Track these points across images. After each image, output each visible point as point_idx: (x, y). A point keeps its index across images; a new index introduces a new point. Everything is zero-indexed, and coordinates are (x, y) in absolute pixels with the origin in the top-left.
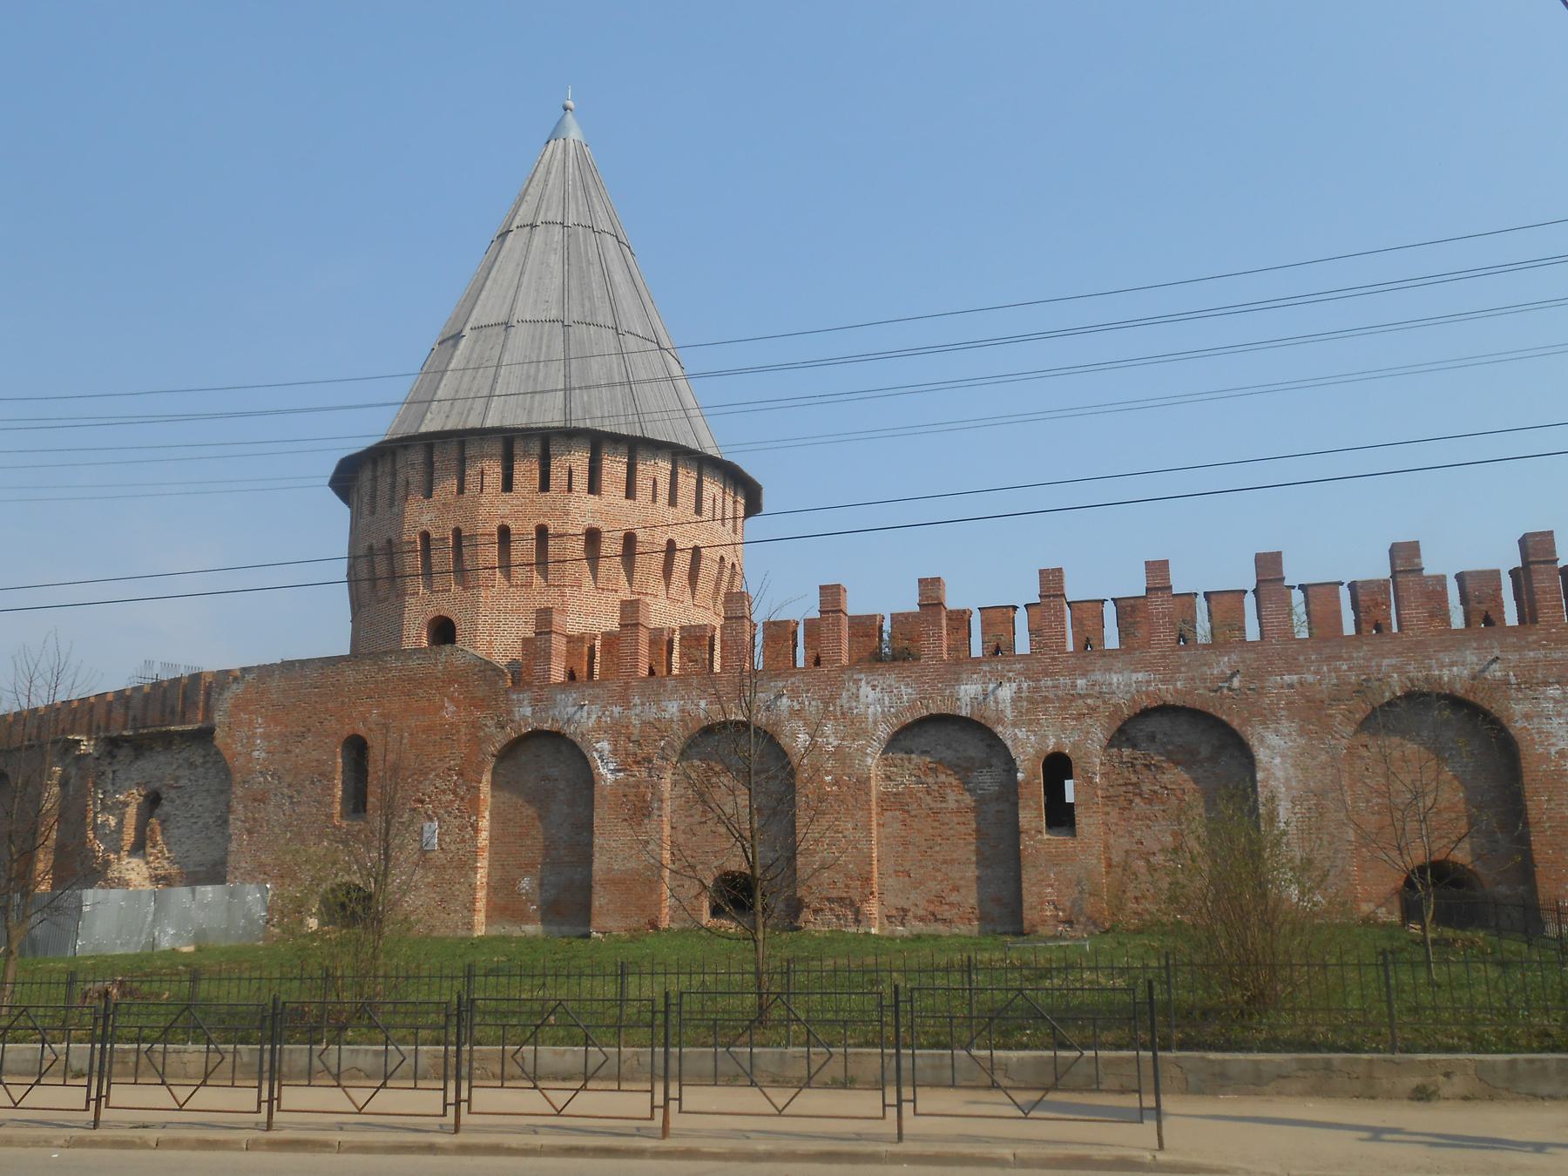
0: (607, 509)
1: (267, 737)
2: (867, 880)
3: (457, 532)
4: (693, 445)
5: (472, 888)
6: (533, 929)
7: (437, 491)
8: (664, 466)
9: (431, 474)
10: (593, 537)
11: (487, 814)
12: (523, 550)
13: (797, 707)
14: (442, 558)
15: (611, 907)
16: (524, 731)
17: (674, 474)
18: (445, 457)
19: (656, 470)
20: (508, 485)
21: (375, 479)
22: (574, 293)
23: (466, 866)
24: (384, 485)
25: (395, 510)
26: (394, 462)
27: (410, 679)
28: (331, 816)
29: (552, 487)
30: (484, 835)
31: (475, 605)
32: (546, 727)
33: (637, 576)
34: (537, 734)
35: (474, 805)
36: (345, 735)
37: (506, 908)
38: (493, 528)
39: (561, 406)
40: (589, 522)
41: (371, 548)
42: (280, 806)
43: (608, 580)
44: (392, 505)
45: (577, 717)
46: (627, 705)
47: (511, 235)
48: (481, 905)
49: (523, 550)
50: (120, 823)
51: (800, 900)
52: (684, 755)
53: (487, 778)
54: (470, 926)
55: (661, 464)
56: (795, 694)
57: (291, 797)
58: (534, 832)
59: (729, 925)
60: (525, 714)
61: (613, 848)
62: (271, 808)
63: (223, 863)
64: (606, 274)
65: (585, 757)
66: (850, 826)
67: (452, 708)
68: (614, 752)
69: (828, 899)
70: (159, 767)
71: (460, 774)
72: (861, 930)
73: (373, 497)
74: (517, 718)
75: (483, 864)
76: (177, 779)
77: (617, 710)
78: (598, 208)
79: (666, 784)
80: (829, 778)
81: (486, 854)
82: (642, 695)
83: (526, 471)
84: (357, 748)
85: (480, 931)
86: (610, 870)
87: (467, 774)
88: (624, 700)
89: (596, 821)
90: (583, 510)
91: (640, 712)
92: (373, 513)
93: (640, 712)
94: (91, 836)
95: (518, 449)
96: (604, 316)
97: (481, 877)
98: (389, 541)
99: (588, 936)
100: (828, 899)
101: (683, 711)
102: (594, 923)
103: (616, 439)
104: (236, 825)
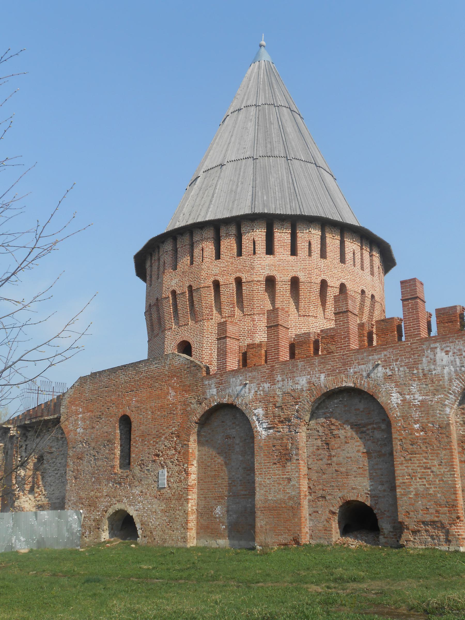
0: (281, 264)
1: (84, 419)
2: (453, 506)
4: (337, 218)
5: (186, 513)
6: (223, 542)
7: (180, 265)
9: (176, 258)
10: (270, 282)
11: (195, 463)
12: (228, 291)
13: (390, 373)
15: (268, 527)
16: (212, 405)
19: (310, 236)
20: (218, 256)
23: (182, 498)
25: (159, 280)
27: (152, 377)
28: (113, 467)
29: (244, 253)
31: (202, 332)
32: (225, 401)
33: (302, 305)
34: (221, 407)
35: (185, 456)
36: (120, 416)
37: (208, 527)
38: (210, 283)
39: (250, 204)
40: (268, 272)
42: (89, 462)
45: (243, 392)
46: (273, 382)
47: (228, 118)
49: (228, 291)
51: (401, 523)
52: (313, 415)
53: (193, 438)
54: (185, 539)
55: (313, 231)
56: (387, 363)
57: (94, 456)
58: (222, 474)
59: (353, 543)
60: (214, 394)
61: (268, 485)
63: (64, 498)
64: (282, 128)
65: (248, 420)
66: (436, 463)
67: (173, 394)
68: (266, 415)
69: (423, 523)
71: (178, 436)
72: (452, 549)
74: (208, 397)
75: (193, 497)
77: (267, 385)
78: (278, 93)
79: (302, 435)
80: (417, 426)
81: (195, 490)
83: (229, 244)
84: (126, 422)
85: (192, 543)
86: (266, 500)
87: (181, 436)
88: (271, 379)
89: (257, 465)
90: (263, 265)
91: (282, 386)
93: (282, 386)
94: (14, 482)
97: (192, 504)
98: (157, 299)
99: (254, 548)
100: (423, 523)
101: (309, 383)
102: (257, 539)
103: (283, 219)
104: (70, 475)
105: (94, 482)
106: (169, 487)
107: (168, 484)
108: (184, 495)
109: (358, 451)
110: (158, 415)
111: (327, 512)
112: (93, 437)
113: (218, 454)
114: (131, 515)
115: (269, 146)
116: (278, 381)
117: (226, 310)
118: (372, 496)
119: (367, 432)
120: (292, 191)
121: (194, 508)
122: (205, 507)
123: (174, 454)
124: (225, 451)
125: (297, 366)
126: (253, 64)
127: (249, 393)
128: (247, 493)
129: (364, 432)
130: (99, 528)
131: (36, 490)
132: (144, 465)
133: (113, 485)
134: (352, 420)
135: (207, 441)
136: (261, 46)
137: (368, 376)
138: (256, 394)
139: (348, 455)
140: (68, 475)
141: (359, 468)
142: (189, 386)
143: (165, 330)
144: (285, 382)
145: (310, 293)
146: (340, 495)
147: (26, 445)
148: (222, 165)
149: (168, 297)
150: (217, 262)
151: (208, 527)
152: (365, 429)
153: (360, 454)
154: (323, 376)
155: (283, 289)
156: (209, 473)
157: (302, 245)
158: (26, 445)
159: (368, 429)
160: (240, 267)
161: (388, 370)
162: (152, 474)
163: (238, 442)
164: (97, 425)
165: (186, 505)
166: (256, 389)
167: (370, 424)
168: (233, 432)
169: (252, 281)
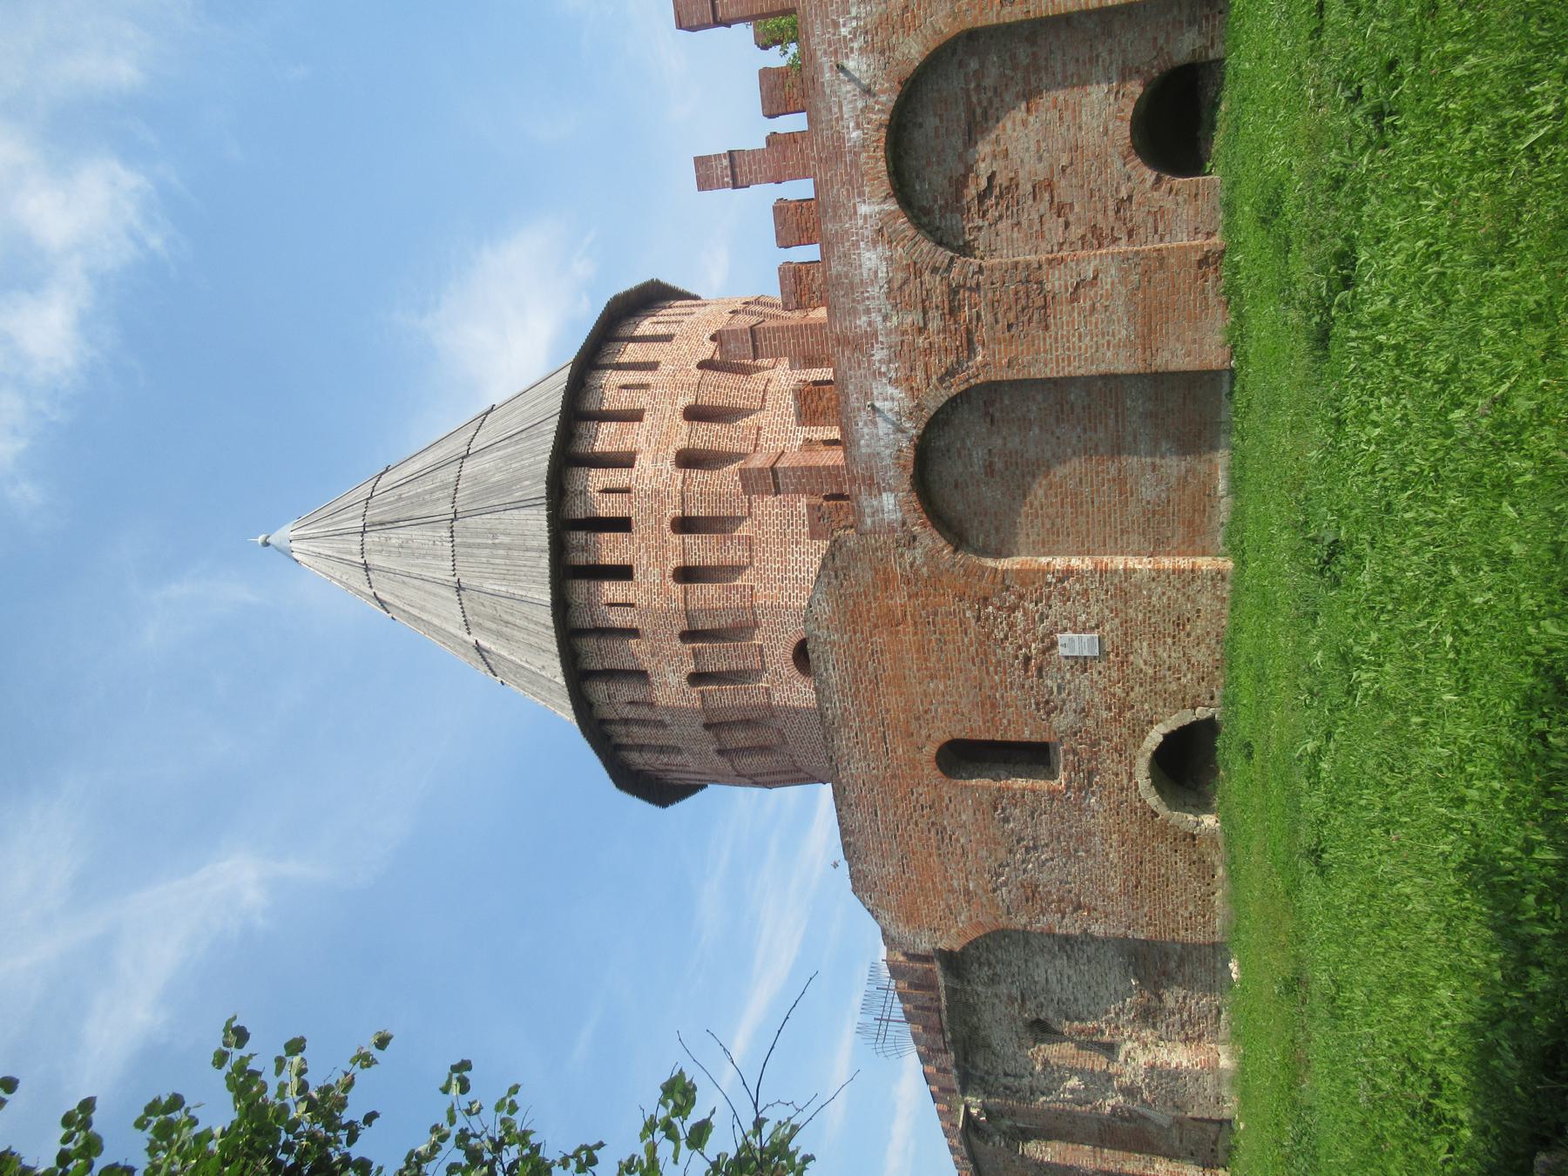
3: (687, 636)
8: (611, 379)
10: (688, 460)
11: (1044, 560)
12: (701, 549)
14: (717, 657)
15: (1189, 335)
17: (620, 367)
18: (597, 654)
19: (611, 388)
21: (641, 748)
22: (424, 512)
23: (1122, 588)
24: (640, 734)
25: (667, 719)
26: (612, 722)
28: (1053, 795)
30: (1075, 562)
31: (776, 610)
33: (741, 403)
35: (1023, 576)
38: (677, 589)
40: (669, 465)
41: (721, 752)
43: (744, 439)
44: (661, 724)
47: (380, 595)
48: (1184, 563)
49: (701, 549)
50: (1080, 1072)
57: (1027, 850)
60: (890, 505)
62: (1043, 878)
70: (998, 1023)
71: (985, 601)
73: (662, 749)
76: (1012, 999)
77: (879, 354)
82: (854, 312)
83: (610, 548)
84: (962, 756)
86: (1128, 343)
92: (677, 750)
95: (580, 559)
96: (449, 474)
98: (707, 726)
104: (1071, 926)
105: (1087, 852)
106: (1097, 626)
107: (1092, 629)
108: (1116, 581)
109: (1025, 123)
110: (939, 660)
111: (1156, 194)
112: (985, 853)
113: (1025, 497)
114: (1161, 739)
115: (436, 496)
116: (870, 324)
117: (735, 555)
118: (1124, 77)
119: (985, 104)
120: (524, 435)
121: (1145, 560)
122: (1144, 534)
123: (1025, 614)
124: (1019, 475)
125: (839, 276)
126: (295, 555)
127: (893, 399)
128: (1111, 410)
129: (985, 113)
130: (1194, 837)
131: (1106, 1038)
132: (1047, 702)
133: (1093, 793)
134: (957, 141)
135: (997, 530)
136: (266, 544)
137: (867, 91)
138: (896, 380)
139: (1033, 148)
140: (1071, 931)
141: (1061, 118)
142: (876, 571)
143: (770, 705)
144: (872, 304)
145: (723, 389)
146: (1118, 164)
147: (1006, 1075)
148: (459, 588)
149: (702, 692)
150: (638, 576)
151: (1191, 523)
152: (979, 111)
153: (1031, 119)
154: (863, 209)
155: (708, 436)
156: (1068, 522)
157: (623, 401)
158: (1006, 1075)
159: (980, 103)
160: (652, 521)
161: (855, 45)
162: (1068, 676)
163: (1000, 442)
164: (958, 840)
165: (1138, 575)
166: (884, 380)
167: (969, 97)
168: (979, 456)
169: (682, 494)
